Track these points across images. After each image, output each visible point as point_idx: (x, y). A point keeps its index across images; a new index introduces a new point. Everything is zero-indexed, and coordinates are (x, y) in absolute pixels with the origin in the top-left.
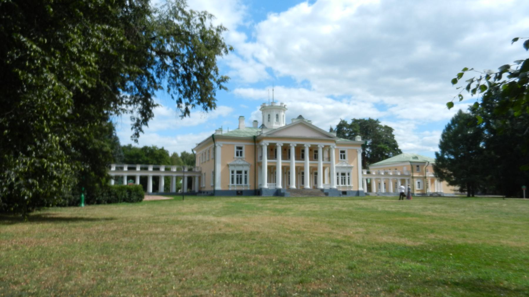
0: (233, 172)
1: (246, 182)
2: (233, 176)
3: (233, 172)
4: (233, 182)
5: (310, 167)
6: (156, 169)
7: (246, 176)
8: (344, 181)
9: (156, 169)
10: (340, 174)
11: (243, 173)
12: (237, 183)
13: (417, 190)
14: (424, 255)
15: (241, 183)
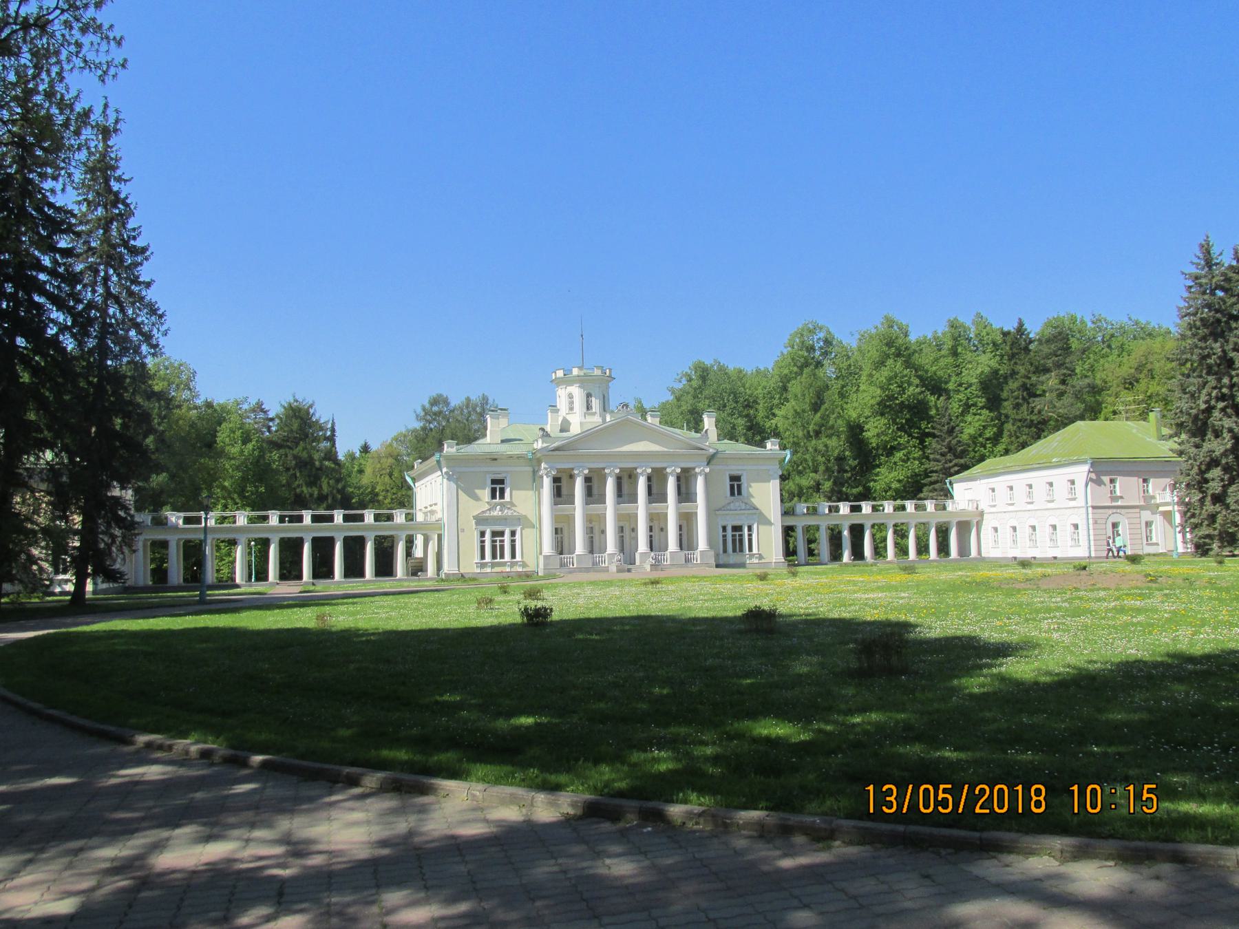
0: (724, 528)
1: (513, 556)
2: (724, 536)
3: (724, 528)
4: (483, 557)
5: (666, 501)
6: (856, 509)
7: (750, 535)
8: (497, 552)
9: (856, 509)
10: (729, 529)
11: (746, 529)
12: (494, 557)
13: (533, 503)
14: (210, 411)
15: (502, 556)
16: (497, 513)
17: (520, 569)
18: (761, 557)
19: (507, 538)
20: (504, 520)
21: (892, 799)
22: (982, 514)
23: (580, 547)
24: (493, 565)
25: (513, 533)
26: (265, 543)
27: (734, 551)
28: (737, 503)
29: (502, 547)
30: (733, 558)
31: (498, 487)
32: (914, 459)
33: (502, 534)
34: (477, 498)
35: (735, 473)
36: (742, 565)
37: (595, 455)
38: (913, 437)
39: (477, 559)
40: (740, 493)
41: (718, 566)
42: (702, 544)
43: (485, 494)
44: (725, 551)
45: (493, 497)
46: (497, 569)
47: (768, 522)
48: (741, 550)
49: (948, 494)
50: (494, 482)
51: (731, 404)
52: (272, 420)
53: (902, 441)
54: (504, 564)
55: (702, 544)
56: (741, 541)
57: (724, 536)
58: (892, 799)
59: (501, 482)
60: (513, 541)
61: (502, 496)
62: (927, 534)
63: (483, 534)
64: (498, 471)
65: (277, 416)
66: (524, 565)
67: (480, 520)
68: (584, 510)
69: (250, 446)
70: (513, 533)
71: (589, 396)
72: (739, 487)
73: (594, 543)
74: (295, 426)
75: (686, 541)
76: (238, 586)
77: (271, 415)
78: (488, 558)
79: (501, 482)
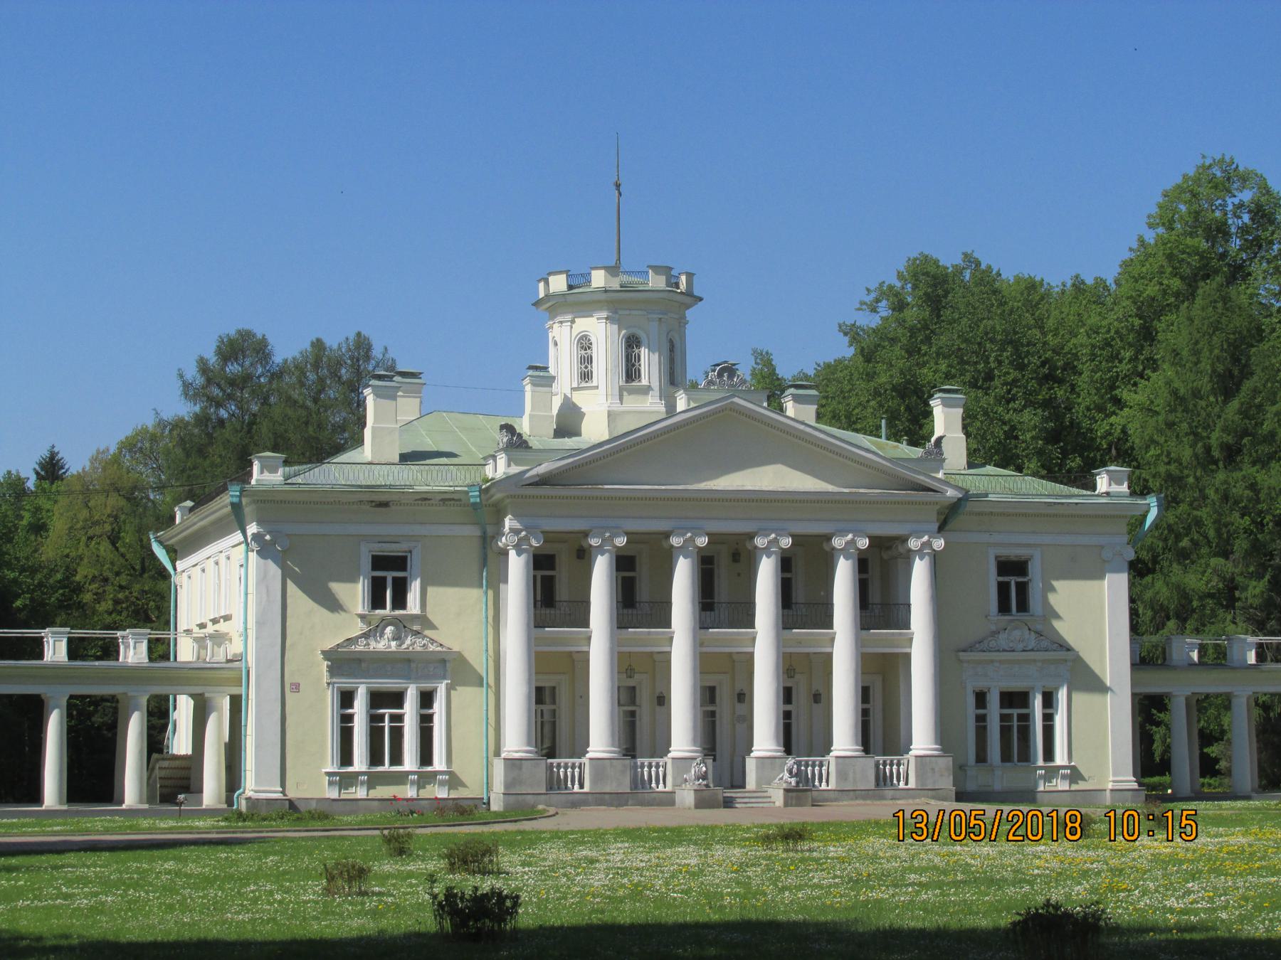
0: (981, 698)
1: (426, 756)
2: (981, 719)
3: (981, 698)
4: (346, 756)
7: (426, 724)
8: (383, 744)
12: (375, 757)
15: (397, 758)
16: (385, 643)
17: (442, 793)
19: (410, 709)
20: (404, 664)
24: (374, 780)
25: (426, 699)
27: (1006, 757)
29: (397, 734)
30: (1003, 777)
31: (389, 576)
33: (396, 699)
34: (333, 605)
35: (1013, 553)
39: (331, 765)
40: (1023, 606)
41: (961, 797)
42: (922, 738)
43: (355, 594)
44: (981, 757)
45: (377, 602)
48: (1025, 755)
50: (380, 562)
54: (401, 778)
55: (922, 738)
56: (1025, 733)
57: (981, 719)
59: (399, 563)
60: (426, 724)
61: (400, 602)
63: (347, 699)
66: (454, 781)
67: (343, 662)
71: (632, 343)
72: (1023, 589)
78: (360, 762)
79: (399, 563)
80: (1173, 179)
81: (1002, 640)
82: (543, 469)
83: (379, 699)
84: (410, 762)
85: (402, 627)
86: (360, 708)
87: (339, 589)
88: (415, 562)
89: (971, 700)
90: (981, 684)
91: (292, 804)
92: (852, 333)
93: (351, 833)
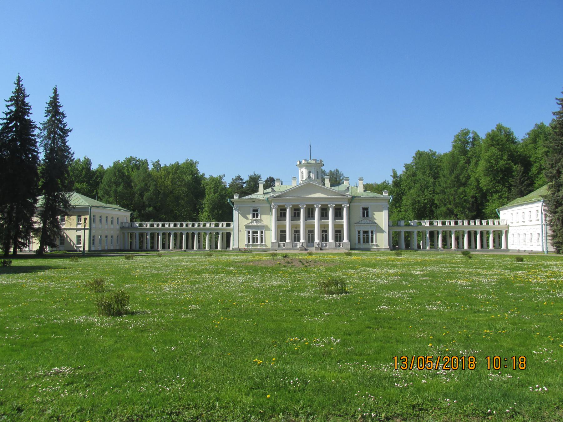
0: (359, 232)
1: (262, 242)
2: (359, 236)
3: (359, 232)
4: (249, 242)
7: (262, 236)
8: (255, 240)
12: (253, 242)
15: (257, 242)
16: (254, 224)
17: (264, 248)
18: (377, 245)
19: (259, 234)
20: (257, 227)
21: (405, 363)
22: (508, 227)
23: (317, 239)
24: (253, 246)
25: (262, 233)
26: (217, 234)
27: (364, 242)
28: (365, 220)
29: (257, 238)
30: (363, 246)
31: (255, 213)
32: (505, 198)
33: (257, 233)
34: (247, 218)
35: (365, 206)
36: (368, 249)
37: (295, 199)
38: (505, 187)
39: (246, 243)
40: (367, 215)
41: (351, 249)
42: (345, 239)
43: (250, 216)
44: (359, 242)
45: (254, 217)
46: (254, 247)
47: (382, 231)
48: (368, 242)
49: (497, 217)
50: (254, 211)
51: (428, 171)
52: (244, 183)
53: (498, 189)
54: (257, 245)
55: (345, 239)
56: (368, 238)
57: (359, 236)
58: (405, 363)
59: (257, 211)
60: (262, 236)
61: (257, 217)
62: (217, 238)
63: (249, 233)
64: (256, 206)
65: (247, 181)
66: (266, 246)
67: (247, 227)
68: (333, 222)
69: (216, 195)
70: (262, 233)
71: (310, 172)
72: (367, 213)
73: (296, 237)
74: (252, 183)
75: (338, 236)
76: (158, 251)
77: (244, 181)
78: (251, 243)
79: (257, 211)
80: (452, 140)
81: (363, 222)
82: (276, 195)
83: (254, 233)
84: (259, 242)
85: (257, 221)
86: (251, 234)
87: (248, 216)
88: (259, 211)
89: (357, 232)
90: (359, 230)
91: (239, 250)
92: (204, 174)
93: (261, 253)
